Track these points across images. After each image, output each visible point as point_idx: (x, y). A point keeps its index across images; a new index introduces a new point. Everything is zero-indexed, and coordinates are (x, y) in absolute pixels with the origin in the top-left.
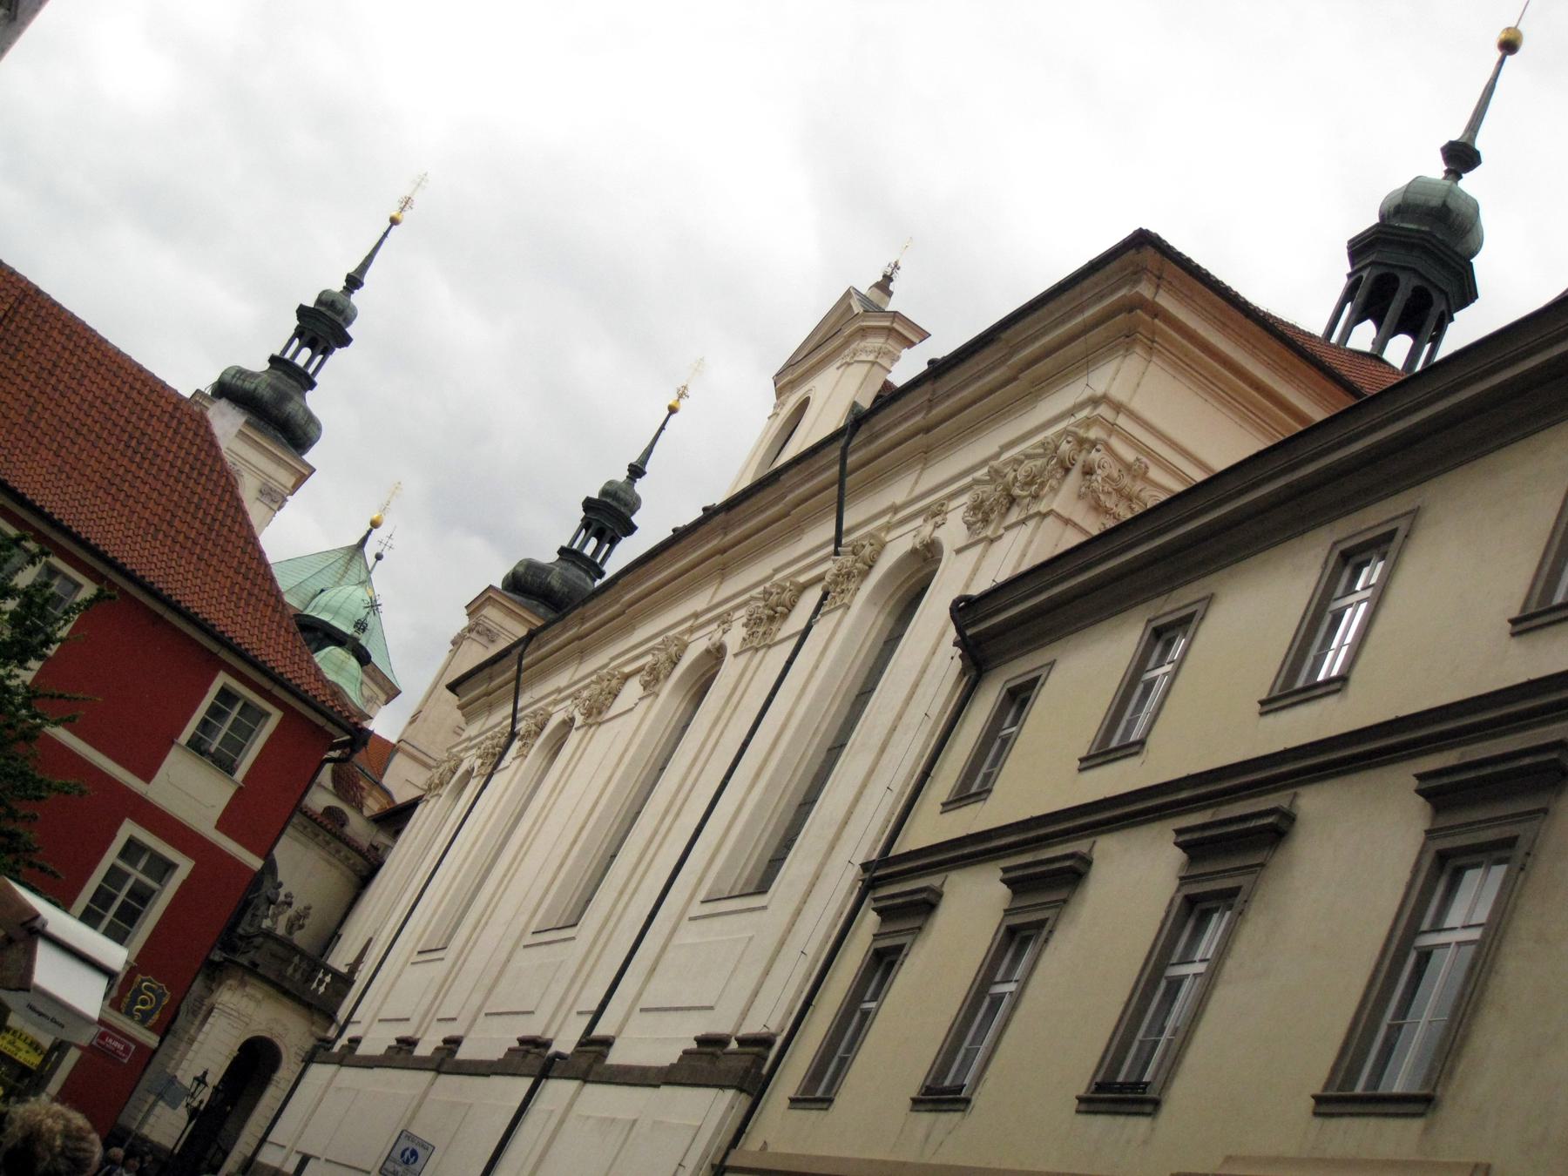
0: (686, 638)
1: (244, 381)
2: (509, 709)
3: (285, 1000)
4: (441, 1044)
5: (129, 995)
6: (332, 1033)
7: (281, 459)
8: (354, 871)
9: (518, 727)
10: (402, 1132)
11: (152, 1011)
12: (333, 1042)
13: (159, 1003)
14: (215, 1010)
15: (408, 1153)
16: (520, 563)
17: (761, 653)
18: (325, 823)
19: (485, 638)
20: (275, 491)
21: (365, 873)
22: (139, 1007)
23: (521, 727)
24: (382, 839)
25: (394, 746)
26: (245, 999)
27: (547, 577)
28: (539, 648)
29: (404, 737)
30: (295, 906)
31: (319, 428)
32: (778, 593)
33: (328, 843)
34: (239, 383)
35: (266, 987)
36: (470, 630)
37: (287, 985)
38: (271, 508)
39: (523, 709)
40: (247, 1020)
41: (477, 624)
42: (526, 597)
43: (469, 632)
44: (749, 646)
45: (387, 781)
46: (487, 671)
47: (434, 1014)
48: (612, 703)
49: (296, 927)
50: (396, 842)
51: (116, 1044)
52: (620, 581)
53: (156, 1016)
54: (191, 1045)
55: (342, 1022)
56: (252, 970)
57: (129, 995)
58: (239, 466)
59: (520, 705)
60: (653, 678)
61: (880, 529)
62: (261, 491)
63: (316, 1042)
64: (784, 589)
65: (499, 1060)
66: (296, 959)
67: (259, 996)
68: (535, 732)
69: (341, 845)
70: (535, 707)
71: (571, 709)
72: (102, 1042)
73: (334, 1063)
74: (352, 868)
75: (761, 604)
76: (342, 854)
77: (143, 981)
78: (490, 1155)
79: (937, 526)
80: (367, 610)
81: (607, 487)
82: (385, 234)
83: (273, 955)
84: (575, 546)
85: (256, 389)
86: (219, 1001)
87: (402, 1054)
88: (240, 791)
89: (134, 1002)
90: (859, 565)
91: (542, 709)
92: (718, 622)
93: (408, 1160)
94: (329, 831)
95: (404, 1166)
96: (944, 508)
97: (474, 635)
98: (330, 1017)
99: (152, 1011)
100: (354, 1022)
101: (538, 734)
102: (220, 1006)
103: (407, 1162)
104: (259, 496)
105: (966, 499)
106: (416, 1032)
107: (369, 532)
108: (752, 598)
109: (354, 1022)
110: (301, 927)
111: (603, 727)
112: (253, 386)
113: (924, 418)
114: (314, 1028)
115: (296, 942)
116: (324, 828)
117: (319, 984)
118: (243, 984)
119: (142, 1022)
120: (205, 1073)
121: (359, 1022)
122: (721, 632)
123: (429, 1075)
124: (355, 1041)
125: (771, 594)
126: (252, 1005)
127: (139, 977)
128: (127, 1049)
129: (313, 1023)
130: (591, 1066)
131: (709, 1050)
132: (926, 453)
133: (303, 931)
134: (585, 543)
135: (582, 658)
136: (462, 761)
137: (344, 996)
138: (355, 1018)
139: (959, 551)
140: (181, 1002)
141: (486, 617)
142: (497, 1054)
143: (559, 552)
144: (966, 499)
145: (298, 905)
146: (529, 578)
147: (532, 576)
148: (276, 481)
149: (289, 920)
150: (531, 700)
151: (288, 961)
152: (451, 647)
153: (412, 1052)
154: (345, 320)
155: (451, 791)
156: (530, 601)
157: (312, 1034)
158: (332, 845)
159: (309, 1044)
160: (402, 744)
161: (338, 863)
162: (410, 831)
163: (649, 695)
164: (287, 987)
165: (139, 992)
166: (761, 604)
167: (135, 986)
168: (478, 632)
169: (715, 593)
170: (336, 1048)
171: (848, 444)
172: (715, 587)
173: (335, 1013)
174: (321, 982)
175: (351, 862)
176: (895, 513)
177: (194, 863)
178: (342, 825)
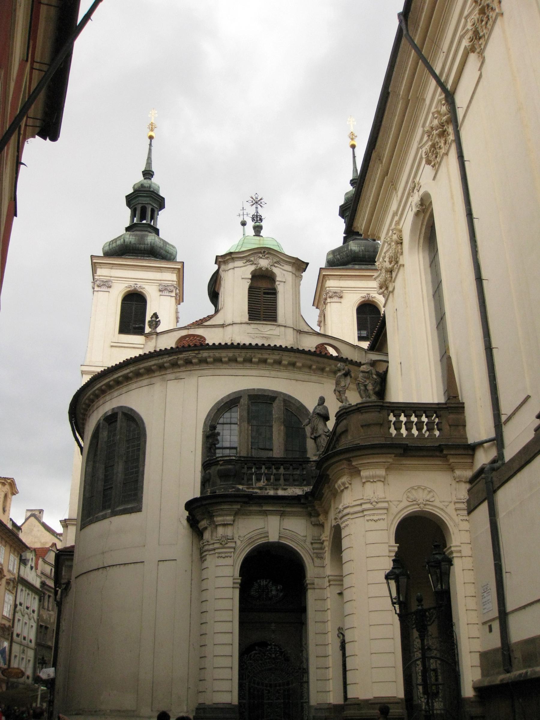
2: (433, 83)
16: (328, 254)
19: (336, 298)
20: (168, 286)
26: (368, 485)
38: (171, 296)
40: (385, 505)
54: (342, 585)
58: (139, 284)
59: (437, 72)
62: (160, 291)
63: (468, 486)
67: (381, 472)
78: (491, 542)
81: (347, 196)
85: (124, 241)
113: (382, 166)
114: (458, 473)
117: (398, 429)
118: (356, 472)
126: (380, 484)
129: (452, 470)
136: (401, 231)
138: (506, 409)
140: (303, 352)
141: (329, 287)
146: (338, 256)
147: (339, 254)
150: (445, 54)
155: (411, 248)
168: (330, 297)
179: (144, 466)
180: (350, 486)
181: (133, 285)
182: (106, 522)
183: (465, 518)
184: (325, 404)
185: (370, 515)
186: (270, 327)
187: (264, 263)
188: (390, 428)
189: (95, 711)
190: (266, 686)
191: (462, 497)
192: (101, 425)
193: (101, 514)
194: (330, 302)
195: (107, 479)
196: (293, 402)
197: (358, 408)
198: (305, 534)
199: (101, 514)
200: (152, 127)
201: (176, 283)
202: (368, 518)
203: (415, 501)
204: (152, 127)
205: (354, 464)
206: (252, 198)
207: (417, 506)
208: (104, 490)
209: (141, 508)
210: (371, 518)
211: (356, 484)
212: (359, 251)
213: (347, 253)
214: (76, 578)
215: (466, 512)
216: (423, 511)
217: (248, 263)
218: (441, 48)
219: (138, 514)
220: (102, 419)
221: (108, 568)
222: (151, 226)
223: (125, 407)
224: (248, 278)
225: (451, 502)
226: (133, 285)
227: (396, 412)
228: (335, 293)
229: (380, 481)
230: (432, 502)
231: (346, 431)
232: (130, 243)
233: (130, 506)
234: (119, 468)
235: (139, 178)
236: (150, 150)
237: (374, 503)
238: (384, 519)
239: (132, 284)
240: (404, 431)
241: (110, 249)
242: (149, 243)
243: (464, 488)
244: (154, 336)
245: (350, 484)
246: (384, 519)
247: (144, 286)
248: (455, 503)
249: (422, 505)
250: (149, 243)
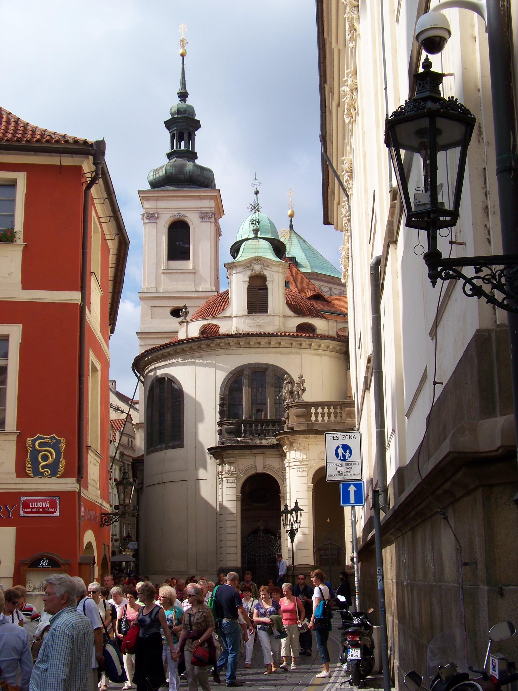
1: (159, 173)
5: (28, 459)
7: (199, 196)
11: (57, 461)
13: (58, 453)
15: (340, 451)
20: (207, 213)
21: (344, 350)
22: (43, 463)
31: (210, 171)
34: (157, 176)
37: (316, 428)
51: (40, 504)
52: (333, 47)
53: (62, 463)
56: (292, 432)
57: (28, 459)
58: (182, 213)
62: (201, 218)
72: (28, 510)
74: (334, 350)
76: (322, 346)
77: (34, 442)
80: (253, 211)
82: (183, 63)
88: (26, 250)
89: (35, 463)
93: (344, 456)
95: (344, 463)
99: (57, 461)
103: (344, 459)
104: (201, 220)
107: (291, 221)
112: (164, 172)
117: (316, 416)
119: (53, 474)
120: (296, 503)
127: (29, 441)
128: (53, 504)
148: (205, 208)
154: (189, 114)
158: (313, 344)
161: (324, 352)
165: (35, 452)
167: (30, 450)
174: (316, 414)
175: (331, 347)
177: (21, 325)
179: (184, 417)
181: (176, 215)
182: (162, 452)
186: (262, 317)
187: (257, 268)
189: (164, 572)
190: (258, 556)
192: (154, 384)
193: (159, 447)
195: (162, 422)
196: (280, 370)
198: (279, 467)
199: (159, 447)
200: (183, 43)
201: (214, 209)
204: (183, 43)
206: (251, 205)
208: (160, 430)
209: (184, 445)
214: (146, 487)
217: (246, 269)
219: (183, 449)
220: (155, 380)
221: (165, 483)
222: (190, 151)
223: (169, 374)
224: (247, 281)
226: (176, 215)
232: (171, 174)
233: (176, 443)
234: (168, 416)
235: (176, 102)
236: (183, 68)
239: (175, 213)
240: (320, 418)
241: (154, 179)
242: (188, 173)
244: (185, 324)
247: (187, 215)
250: (188, 173)
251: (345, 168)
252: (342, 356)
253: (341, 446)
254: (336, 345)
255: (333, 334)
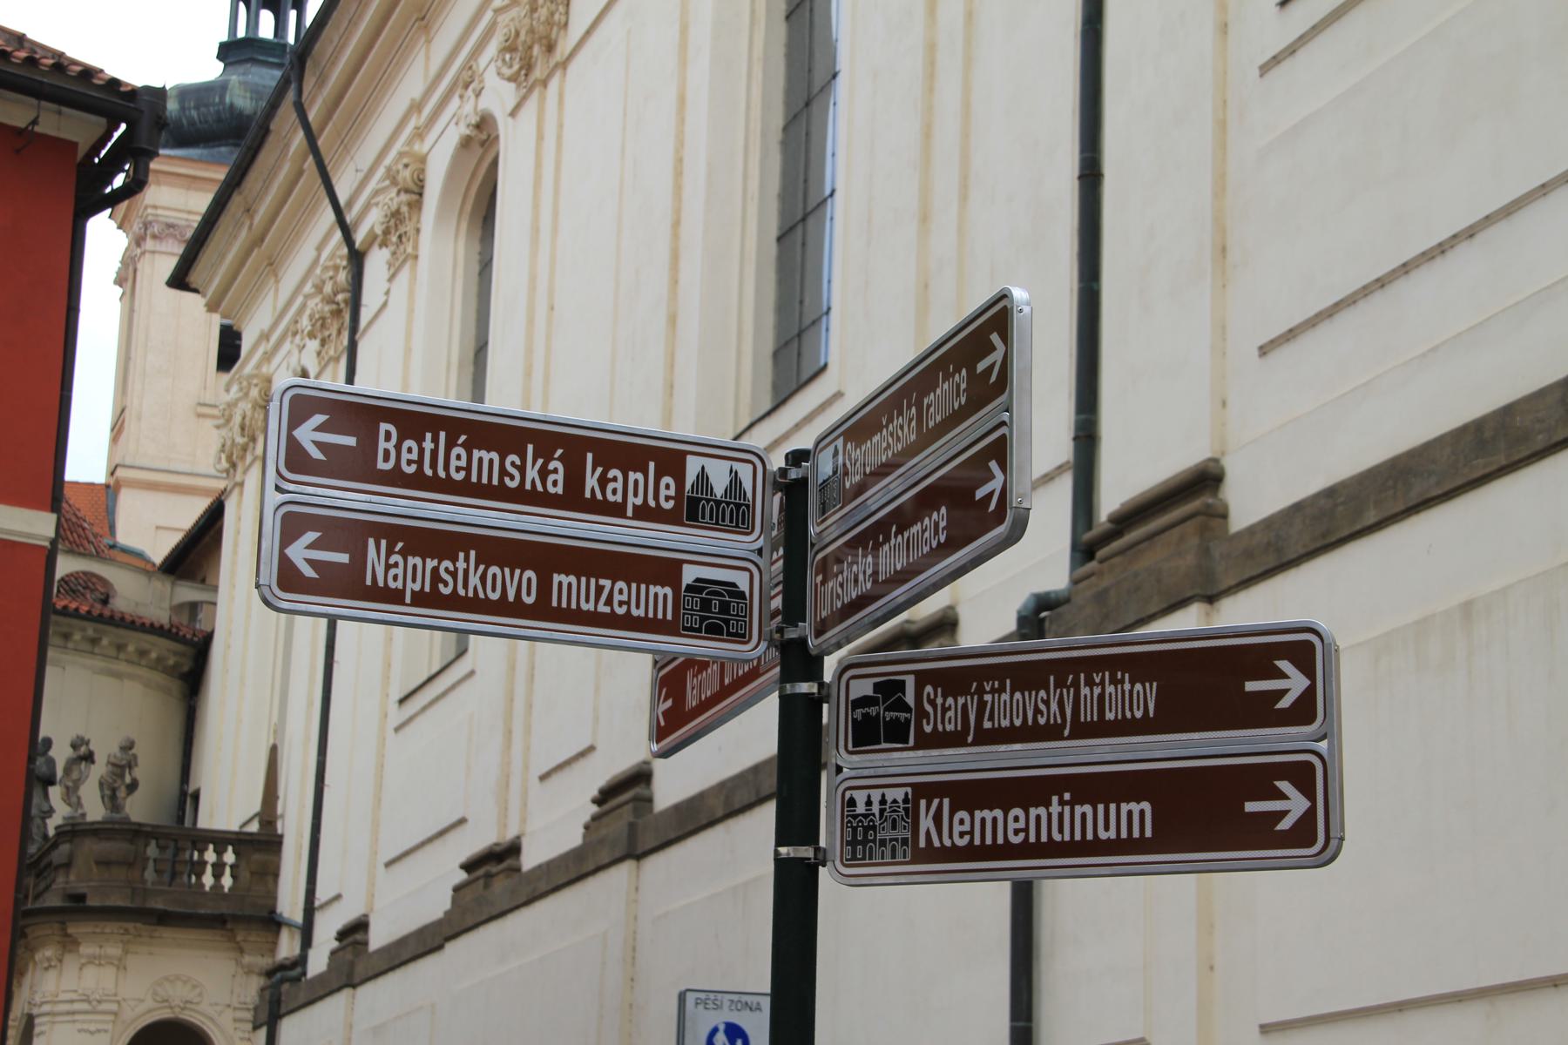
0: (264, 370)
2: (329, 216)
3: (167, 933)
4: (335, 944)
6: (288, 946)
8: (170, 671)
9: (359, 237)
10: (682, 997)
12: (301, 961)
14: (37, 1021)
17: (554, 84)
18: (73, 605)
21: (186, 669)
23: (369, 223)
24: (187, 593)
25: (107, 486)
27: (222, 97)
28: (321, 81)
29: (117, 461)
30: (101, 759)
32: (331, 278)
33: (94, 641)
35: (111, 927)
36: (138, 241)
37: (158, 904)
39: (350, 203)
40: (114, 1007)
41: (146, 225)
42: (204, 147)
43: (138, 244)
44: (326, 359)
45: (123, 538)
46: (237, 201)
47: (526, 767)
48: (567, 13)
49: (122, 793)
50: (215, 589)
55: (298, 918)
56: (77, 907)
60: (398, 228)
61: (410, 142)
64: (336, 268)
65: (446, 913)
66: (152, 851)
67: (114, 950)
68: (410, 205)
69: (122, 632)
70: (388, 161)
71: (469, 108)
73: (339, 989)
74: (158, 665)
75: (318, 299)
76: (131, 648)
79: (478, 94)
83: (104, 863)
84: (241, 33)
86: (38, 999)
87: (500, 885)
90: (404, 197)
91: (401, 155)
92: (289, 339)
94: (88, 617)
96: (299, 326)
97: (149, 244)
98: (272, 923)
100: (322, 907)
101: (416, 205)
102: (46, 1008)
105: (492, 49)
106: (504, 826)
108: (376, 193)
109: (322, 907)
110: (132, 787)
111: (573, 67)
114: (247, 959)
115: (135, 818)
116: (76, 614)
117: (218, 875)
118: (69, 944)
121: (338, 897)
122: (473, 97)
123: (621, 874)
124: (355, 932)
125: (324, 282)
129: (241, 951)
130: (1205, 552)
131: (350, 939)
132: (423, 19)
133: (137, 794)
134: (253, 23)
135: (426, 29)
137: (271, 873)
138: (322, 895)
139: (513, 114)
141: (155, 207)
142: (436, 905)
143: (220, 57)
144: (492, 49)
145: (105, 749)
146: (194, 113)
147: (197, 108)
149: (101, 785)
150: (360, 176)
151: (135, 862)
152: (119, 291)
153: (518, 870)
156: (216, 150)
157: (249, 971)
158: (105, 642)
159: (251, 989)
160: (120, 473)
162: (235, 552)
163: (530, 90)
164: (160, 906)
166: (318, 299)
168: (154, 237)
169: (428, 58)
170: (318, 963)
171: (300, 92)
172: (272, 293)
173: (273, 911)
175: (154, 655)
176: (268, 340)
178: (105, 601)
180: (59, 964)
183: (247, 1035)
184: (52, 753)
185: (84, 1022)
188: (144, 869)
191: (248, 1000)
194: (153, 252)
197: (96, 830)
202: (79, 1026)
203: (167, 1001)
205: (70, 930)
207: (169, 1010)
210: (85, 1026)
211: (71, 962)
212: (255, 113)
213: (218, 112)
215: (249, 1026)
216: (177, 1019)
218: (352, 153)
225: (229, 1006)
227: (162, 842)
228: (170, 226)
229: (112, 964)
230: (197, 1003)
231: (67, 865)
237: (94, 1003)
238: (106, 1031)
243: (256, 983)
245: (60, 961)
246: (106, 1031)
248: (235, 1009)
249: (177, 1010)
251: (405, 179)
252: (176, 686)
253: (722, 1028)
254: (168, 650)
255: (162, 616)
